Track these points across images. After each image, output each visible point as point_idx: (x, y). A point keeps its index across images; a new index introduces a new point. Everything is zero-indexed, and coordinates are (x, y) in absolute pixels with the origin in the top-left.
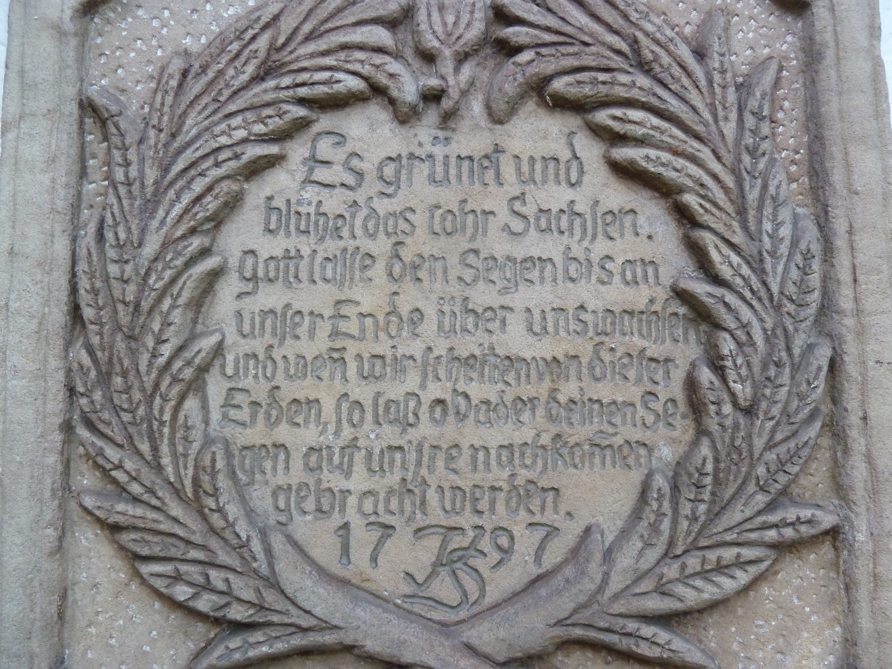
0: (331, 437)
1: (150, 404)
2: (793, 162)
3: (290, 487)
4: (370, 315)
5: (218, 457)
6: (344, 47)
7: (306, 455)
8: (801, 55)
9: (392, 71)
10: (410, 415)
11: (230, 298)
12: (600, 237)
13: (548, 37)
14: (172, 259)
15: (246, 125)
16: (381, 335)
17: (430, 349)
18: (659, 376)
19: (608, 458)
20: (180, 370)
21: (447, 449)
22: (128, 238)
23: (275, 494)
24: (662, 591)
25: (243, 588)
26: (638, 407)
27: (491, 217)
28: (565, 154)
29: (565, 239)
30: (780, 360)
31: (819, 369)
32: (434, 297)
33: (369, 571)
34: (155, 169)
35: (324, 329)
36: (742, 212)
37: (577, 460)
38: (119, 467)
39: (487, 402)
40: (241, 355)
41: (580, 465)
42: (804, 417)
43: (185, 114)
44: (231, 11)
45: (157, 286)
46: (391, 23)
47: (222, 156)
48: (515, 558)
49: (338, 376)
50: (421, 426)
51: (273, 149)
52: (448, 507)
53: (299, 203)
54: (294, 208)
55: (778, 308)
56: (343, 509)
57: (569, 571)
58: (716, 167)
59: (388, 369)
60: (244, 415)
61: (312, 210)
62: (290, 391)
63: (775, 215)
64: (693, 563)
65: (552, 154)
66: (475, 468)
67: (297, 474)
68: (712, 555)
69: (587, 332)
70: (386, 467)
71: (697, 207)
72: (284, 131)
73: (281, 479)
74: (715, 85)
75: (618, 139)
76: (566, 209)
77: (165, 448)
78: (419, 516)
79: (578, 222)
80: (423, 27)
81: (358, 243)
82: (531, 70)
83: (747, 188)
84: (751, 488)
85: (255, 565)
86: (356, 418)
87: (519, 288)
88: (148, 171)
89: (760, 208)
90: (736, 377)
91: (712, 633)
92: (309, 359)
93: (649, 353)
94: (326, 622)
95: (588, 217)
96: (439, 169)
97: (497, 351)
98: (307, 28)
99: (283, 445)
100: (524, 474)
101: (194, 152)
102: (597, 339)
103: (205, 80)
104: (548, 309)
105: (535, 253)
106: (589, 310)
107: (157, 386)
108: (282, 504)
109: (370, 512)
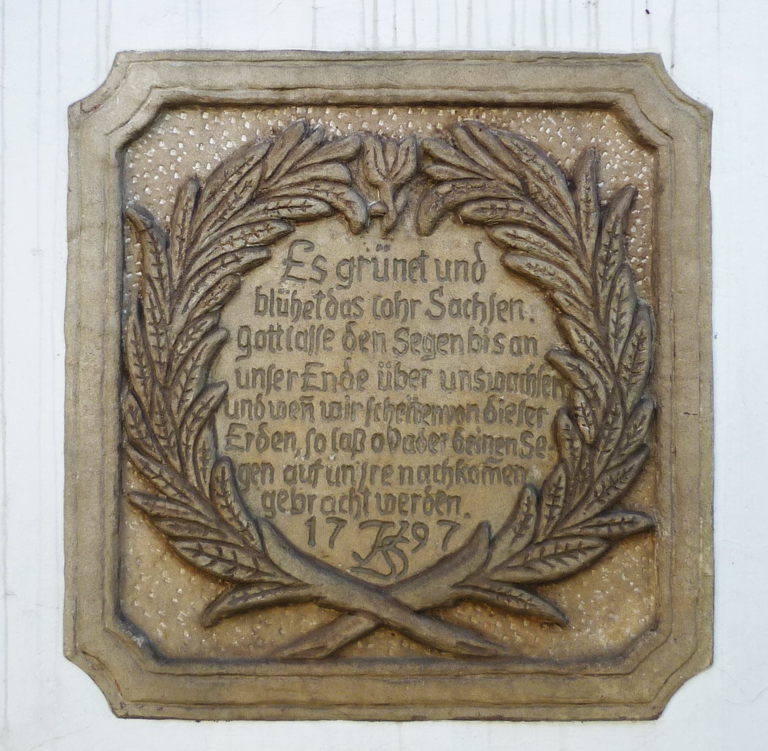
0: (303, 458)
1: (179, 435)
2: (640, 266)
3: (274, 492)
4: (330, 373)
5: (227, 471)
6: (313, 180)
7: (285, 471)
8: (652, 184)
9: (348, 199)
10: (358, 444)
11: (232, 360)
12: (496, 319)
13: (462, 174)
14: (193, 333)
15: (244, 237)
16: (338, 387)
17: (373, 398)
18: (534, 420)
19: (496, 476)
20: (200, 411)
21: (383, 468)
22: (162, 317)
23: (264, 497)
24: (527, 567)
25: (246, 560)
26: (519, 441)
27: (417, 305)
28: (472, 259)
29: (470, 321)
30: (616, 410)
31: (644, 417)
32: (376, 361)
33: (328, 550)
34: (180, 268)
35: (298, 384)
36: (595, 305)
37: (474, 477)
38: (160, 476)
39: (413, 436)
40: (239, 400)
41: (476, 481)
42: (631, 450)
43: (200, 229)
44: (229, 145)
45: (183, 352)
46: (346, 161)
47: (227, 261)
48: (430, 543)
49: (308, 416)
50: (366, 452)
51: (264, 254)
52: (383, 507)
53: (280, 292)
54: (276, 295)
55: (617, 374)
56: (310, 509)
57: (465, 553)
58: (577, 272)
59: (343, 412)
60: (242, 442)
61: (289, 297)
62: (273, 427)
63: (619, 308)
64: (550, 549)
65: (462, 258)
66: (402, 482)
67: (279, 484)
68: (563, 544)
69: (484, 387)
70: (341, 480)
71: (563, 301)
72: (270, 240)
73: (268, 487)
74: (581, 212)
75: (509, 249)
76: (472, 299)
77: (190, 464)
78: (363, 514)
79: (479, 310)
80: (371, 165)
81: (322, 321)
82: (449, 199)
83: (600, 288)
84: (592, 498)
85: (252, 543)
86: (320, 446)
87: (437, 356)
88: (174, 269)
89: (609, 303)
90: (584, 422)
91: (564, 597)
92: (288, 404)
93: (528, 404)
94: (300, 581)
95: (488, 305)
96: (381, 268)
97: (419, 401)
98: (287, 165)
99: (269, 463)
100: (435, 487)
101: (207, 256)
102: (491, 393)
103: (213, 204)
104: (456, 371)
105: (448, 331)
106: (486, 372)
107: (183, 421)
108: (268, 504)
109: (330, 510)
